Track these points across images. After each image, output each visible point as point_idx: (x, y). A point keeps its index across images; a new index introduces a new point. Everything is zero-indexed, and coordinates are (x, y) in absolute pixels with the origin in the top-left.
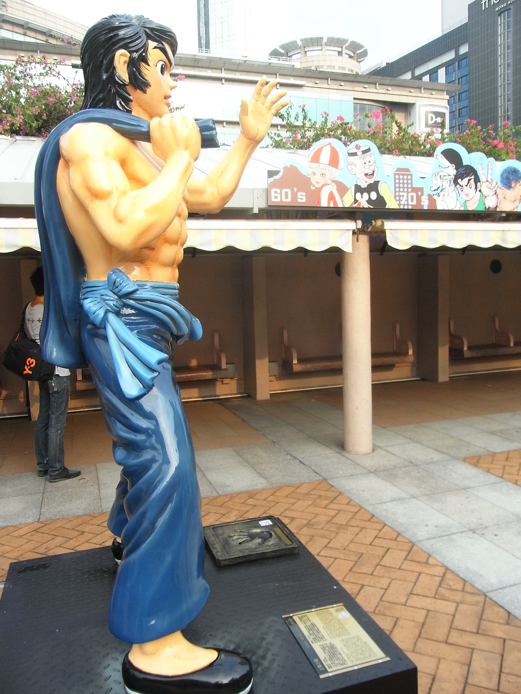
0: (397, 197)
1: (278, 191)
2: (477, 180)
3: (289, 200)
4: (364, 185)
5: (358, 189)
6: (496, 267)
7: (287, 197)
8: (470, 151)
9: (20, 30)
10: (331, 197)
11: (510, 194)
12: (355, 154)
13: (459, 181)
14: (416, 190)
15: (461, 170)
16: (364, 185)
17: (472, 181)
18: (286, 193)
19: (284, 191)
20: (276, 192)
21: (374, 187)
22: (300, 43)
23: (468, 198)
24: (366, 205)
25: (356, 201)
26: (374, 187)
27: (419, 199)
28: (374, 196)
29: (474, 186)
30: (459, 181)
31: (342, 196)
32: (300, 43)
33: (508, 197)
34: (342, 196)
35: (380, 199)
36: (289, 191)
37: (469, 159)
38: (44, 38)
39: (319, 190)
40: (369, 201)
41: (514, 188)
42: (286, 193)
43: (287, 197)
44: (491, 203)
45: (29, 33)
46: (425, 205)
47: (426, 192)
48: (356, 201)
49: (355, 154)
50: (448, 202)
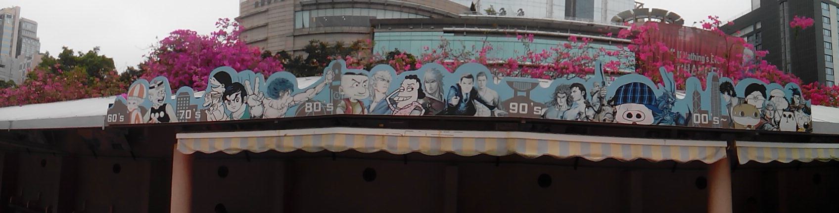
0: (178, 114)
1: (516, 104)
2: (244, 93)
3: (526, 112)
4: (157, 108)
5: (153, 111)
6: (545, 181)
7: (523, 110)
8: (239, 70)
9: (413, 11)
10: (137, 117)
11: (277, 103)
12: (153, 87)
13: (228, 97)
14: (191, 108)
15: (230, 88)
16: (157, 108)
17: (239, 96)
18: (524, 107)
19: (521, 105)
20: (514, 106)
21: (163, 108)
22: (650, 11)
23: (237, 109)
24: (157, 122)
25: (151, 119)
26: (163, 108)
27: (193, 114)
28: (162, 114)
29: (240, 100)
30: (228, 97)
31: (143, 115)
32: (650, 11)
33: (275, 106)
34: (143, 115)
35: (166, 116)
36: (526, 105)
37: (236, 77)
38: (429, 14)
39: (130, 113)
40: (159, 118)
41: (282, 97)
42: (524, 107)
43: (523, 110)
44: (256, 112)
45: (420, 13)
46: (198, 117)
47: (199, 108)
48: (151, 119)
49: (153, 87)
50: (217, 114)
